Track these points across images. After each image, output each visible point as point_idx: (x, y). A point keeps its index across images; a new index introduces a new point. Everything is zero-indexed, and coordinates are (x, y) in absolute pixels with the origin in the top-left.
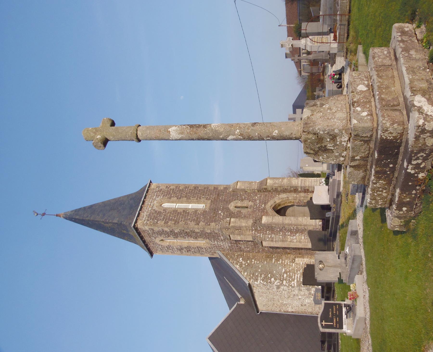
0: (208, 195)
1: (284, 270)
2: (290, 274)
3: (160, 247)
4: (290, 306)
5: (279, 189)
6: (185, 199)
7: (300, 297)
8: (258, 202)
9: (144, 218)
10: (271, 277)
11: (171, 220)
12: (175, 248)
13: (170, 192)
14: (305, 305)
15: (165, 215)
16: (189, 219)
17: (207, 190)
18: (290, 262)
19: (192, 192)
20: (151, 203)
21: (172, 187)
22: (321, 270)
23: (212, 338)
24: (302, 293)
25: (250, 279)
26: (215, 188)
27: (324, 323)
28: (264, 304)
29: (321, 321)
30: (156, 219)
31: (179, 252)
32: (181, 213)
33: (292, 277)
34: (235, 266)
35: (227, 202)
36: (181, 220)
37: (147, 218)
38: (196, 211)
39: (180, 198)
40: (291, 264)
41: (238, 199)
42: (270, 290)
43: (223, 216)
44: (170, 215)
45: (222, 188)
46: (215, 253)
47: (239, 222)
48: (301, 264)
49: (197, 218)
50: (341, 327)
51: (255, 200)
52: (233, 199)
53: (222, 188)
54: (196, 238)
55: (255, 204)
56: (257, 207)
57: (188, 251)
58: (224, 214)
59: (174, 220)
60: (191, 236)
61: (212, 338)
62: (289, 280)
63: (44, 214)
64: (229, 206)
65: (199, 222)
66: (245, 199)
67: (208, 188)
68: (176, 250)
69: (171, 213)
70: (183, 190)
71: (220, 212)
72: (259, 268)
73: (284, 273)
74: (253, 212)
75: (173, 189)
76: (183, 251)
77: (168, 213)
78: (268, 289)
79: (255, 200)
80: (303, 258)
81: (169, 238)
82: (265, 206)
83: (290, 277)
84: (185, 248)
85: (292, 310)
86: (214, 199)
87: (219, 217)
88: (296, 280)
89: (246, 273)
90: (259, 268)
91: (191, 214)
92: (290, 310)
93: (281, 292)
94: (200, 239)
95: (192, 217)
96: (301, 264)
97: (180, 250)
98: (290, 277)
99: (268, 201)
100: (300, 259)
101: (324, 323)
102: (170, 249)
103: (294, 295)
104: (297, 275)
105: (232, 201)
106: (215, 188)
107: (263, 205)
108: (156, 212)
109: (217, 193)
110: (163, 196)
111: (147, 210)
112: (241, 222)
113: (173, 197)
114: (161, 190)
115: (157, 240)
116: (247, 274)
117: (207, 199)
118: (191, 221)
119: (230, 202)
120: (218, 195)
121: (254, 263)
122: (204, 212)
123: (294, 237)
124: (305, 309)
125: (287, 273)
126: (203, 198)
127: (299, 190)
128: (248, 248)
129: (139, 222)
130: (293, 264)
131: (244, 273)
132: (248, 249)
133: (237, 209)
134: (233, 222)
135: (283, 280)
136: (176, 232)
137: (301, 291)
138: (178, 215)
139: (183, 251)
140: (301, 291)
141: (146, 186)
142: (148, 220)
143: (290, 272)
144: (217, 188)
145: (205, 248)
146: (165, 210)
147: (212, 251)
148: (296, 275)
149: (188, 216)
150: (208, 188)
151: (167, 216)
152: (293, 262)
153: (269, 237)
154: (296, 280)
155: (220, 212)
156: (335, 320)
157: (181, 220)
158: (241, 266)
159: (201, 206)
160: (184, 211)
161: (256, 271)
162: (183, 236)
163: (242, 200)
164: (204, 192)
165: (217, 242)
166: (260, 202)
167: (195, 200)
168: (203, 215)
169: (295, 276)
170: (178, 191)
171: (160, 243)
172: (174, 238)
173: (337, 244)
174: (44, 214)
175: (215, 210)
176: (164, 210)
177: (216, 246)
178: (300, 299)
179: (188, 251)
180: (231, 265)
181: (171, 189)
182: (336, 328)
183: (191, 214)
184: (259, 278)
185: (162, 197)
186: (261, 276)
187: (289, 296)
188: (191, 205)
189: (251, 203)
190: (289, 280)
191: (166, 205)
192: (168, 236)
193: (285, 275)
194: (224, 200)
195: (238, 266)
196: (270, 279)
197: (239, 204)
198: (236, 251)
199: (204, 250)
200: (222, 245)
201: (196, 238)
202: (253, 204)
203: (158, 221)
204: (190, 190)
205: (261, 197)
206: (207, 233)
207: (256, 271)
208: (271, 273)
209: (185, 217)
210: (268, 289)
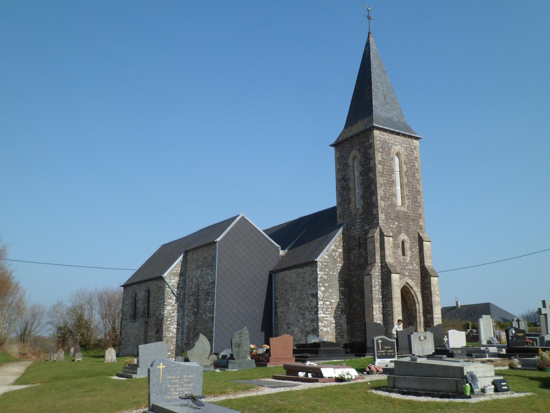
0: (412, 208)
1: (333, 301)
2: (330, 308)
3: (346, 155)
4: (285, 310)
5: (427, 292)
7: (301, 321)
8: (411, 267)
9: (382, 136)
10: (325, 287)
11: (383, 168)
12: (346, 172)
13: (411, 162)
14: (289, 328)
15: (387, 160)
16: (386, 189)
17: (417, 206)
18: (342, 308)
19: (414, 188)
20: (399, 142)
22: (420, 337)
24: (308, 324)
25: (322, 262)
26: (421, 215)
27: (380, 341)
28: (286, 279)
29: (381, 339)
30: (382, 150)
31: (341, 177)
32: (391, 178)
33: (327, 311)
34: (333, 244)
36: (384, 180)
37: (382, 139)
38: (395, 195)
40: (340, 310)
41: (411, 243)
42: (308, 286)
43: (392, 228)
44: (387, 166)
45: (421, 223)
46: (344, 219)
47: (389, 247)
48: (341, 321)
49: (388, 198)
50: (379, 357)
51: (412, 264)
52: (411, 237)
53: (421, 223)
54: (363, 197)
55: (407, 264)
56: (405, 266)
57: (343, 187)
58: (395, 228)
59: (383, 171)
60: (364, 192)
62: (324, 308)
63: (369, 18)
64: (403, 234)
65: (384, 201)
66: (412, 252)
67: (420, 206)
68: (344, 174)
69: (390, 166)
70: (415, 177)
71: (396, 223)
72: (333, 272)
73: (331, 302)
74: (400, 263)
75: (414, 166)
76: (342, 182)
77: (390, 163)
78: (310, 284)
79: (412, 264)
80: (347, 324)
81: (360, 166)
82: (408, 276)
84: (348, 185)
85: (279, 313)
86: (409, 216)
87: (390, 222)
88: (324, 315)
89: (326, 257)
90: (333, 272)
91: (391, 190)
92: (279, 310)
93: (306, 298)
94: (361, 202)
95: (388, 192)
96: (341, 321)
97: (343, 178)
98: (327, 309)
99: (412, 279)
100: (345, 320)
101: (380, 341)
102: (343, 167)
103: (304, 315)
104: (330, 317)
105: (409, 237)
106: (421, 215)
107: (407, 274)
108: (390, 149)
109: (416, 218)
110: (406, 155)
111: (390, 138)
112: (389, 249)
113: (407, 167)
114: (413, 152)
115: (354, 152)
116: (326, 259)
117: (408, 207)
118: (384, 191)
119: (408, 234)
120: (414, 220)
121: (338, 266)
123: (378, 312)
124: (282, 328)
125: (330, 305)
126: (409, 202)
127: (429, 316)
128: (355, 258)
130: (339, 312)
131: (327, 255)
132: (352, 258)
133: (400, 243)
134: (388, 240)
135: (324, 301)
136: (370, 174)
137: (312, 323)
138: (389, 175)
139: (342, 182)
140: (312, 323)
141: (412, 132)
142: (380, 141)
144: (420, 218)
145: (349, 208)
146: (392, 159)
147: (345, 216)
148: (329, 316)
149: (389, 186)
151: (387, 162)
152: (342, 312)
153: (376, 283)
154: (324, 315)
155: (396, 223)
156: (383, 351)
157: (384, 180)
158: (334, 251)
161: (330, 269)
162: (364, 183)
164: (416, 203)
165: (360, 222)
166: (411, 270)
169: (328, 314)
170: (413, 171)
171: (352, 155)
172: (361, 172)
174: (369, 18)
175: (397, 217)
176: (392, 158)
177: (354, 221)
178: (298, 321)
179: (343, 187)
180: (334, 239)
181: (414, 163)
182: (378, 353)
183: (391, 190)
184: (323, 273)
185: (405, 153)
186: (325, 275)
187: (301, 309)
188: (399, 188)
189: (408, 259)
190: (324, 308)
192: (362, 166)
193: (328, 303)
194: (408, 228)
195: (333, 247)
196: (323, 286)
197: (407, 246)
198: (348, 244)
199: (346, 207)
200: (356, 228)
201: (364, 197)
202: (408, 261)
203: (381, 152)
204: (416, 186)
205: (416, 270)
206: (372, 210)
209: (388, 184)
210: (310, 284)
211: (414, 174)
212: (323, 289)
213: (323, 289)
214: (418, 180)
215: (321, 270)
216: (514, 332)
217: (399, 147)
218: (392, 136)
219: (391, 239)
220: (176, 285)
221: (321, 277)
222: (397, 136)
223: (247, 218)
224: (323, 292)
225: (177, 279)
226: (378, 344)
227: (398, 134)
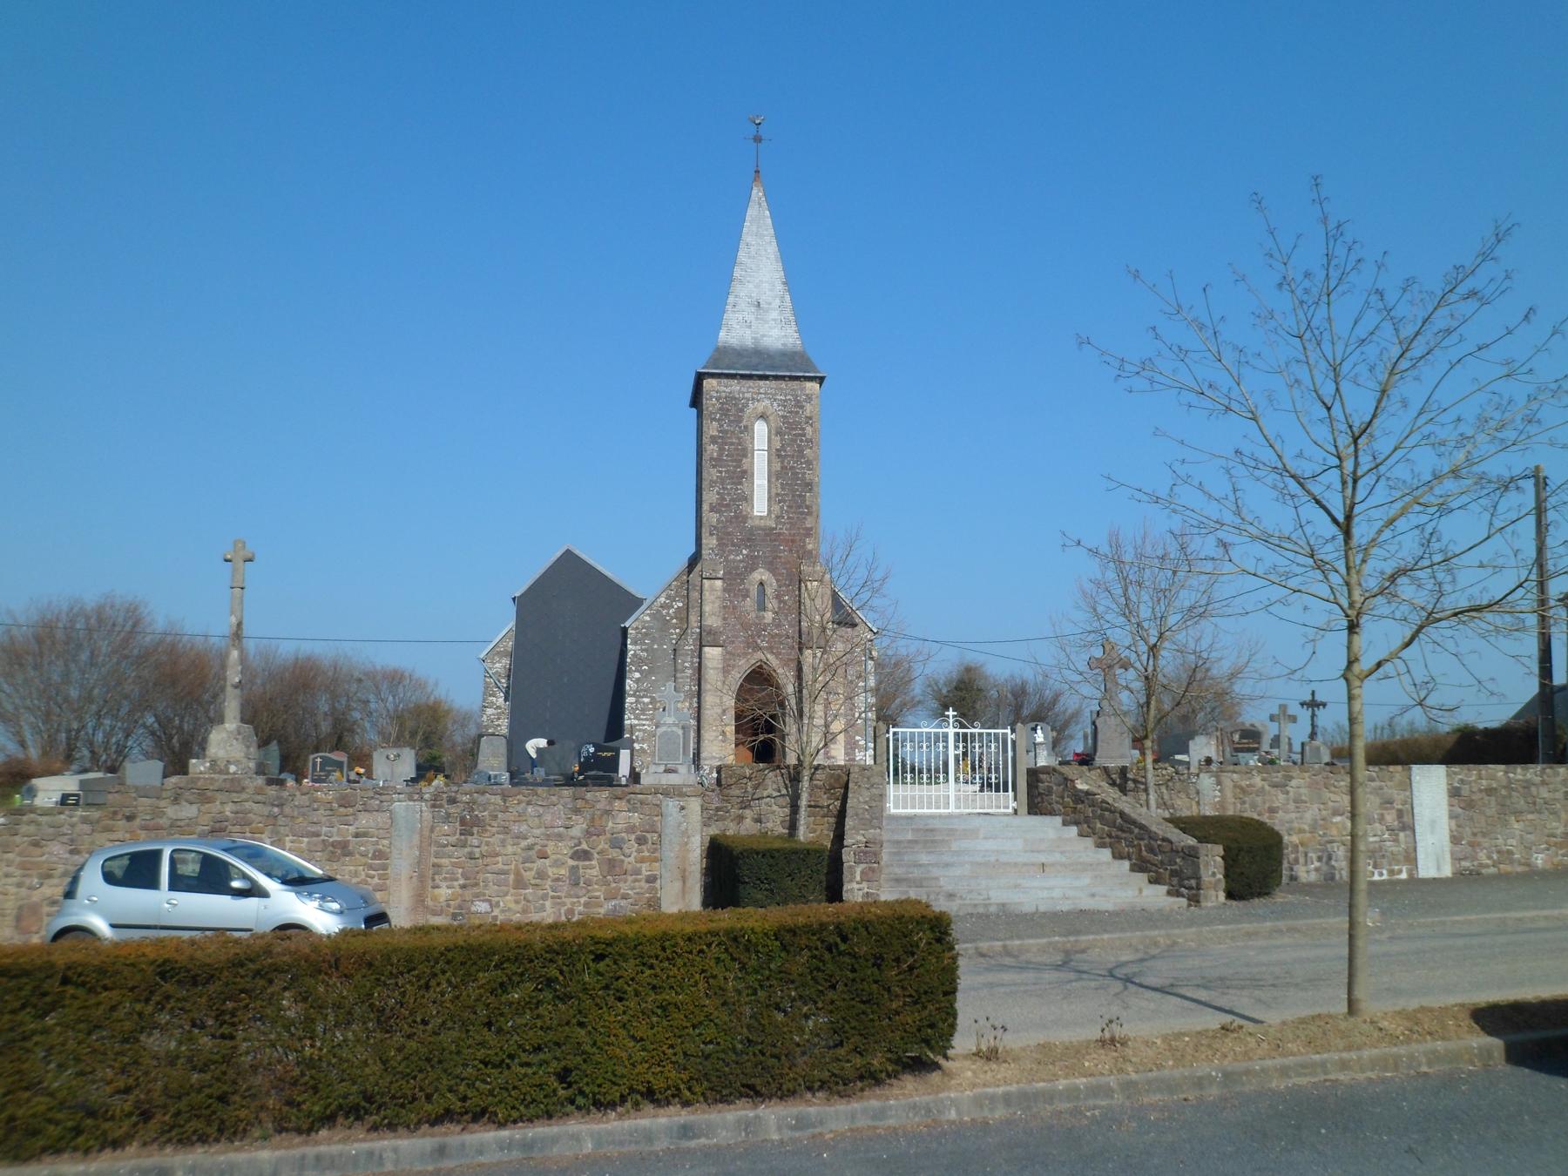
6: (777, 466)
11: (721, 449)
21: (809, 430)
23: (568, 552)
35: (771, 563)
38: (747, 499)
39: (779, 456)
49: (728, 505)
59: (720, 455)
61: (568, 552)
63: (758, 139)
70: (803, 456)
72: (661, 645)
73: (653, 698)
83: (643, 711)
90: (661, 645)
99: (777, 655)
108: (742, 410)
114: (802, 407)
122: (741, 518)
129: (714, 382)
143: (655, 709)
146: (748, 429)
150: (809, 513)
159: (760, 506)
160: (745, 472)
161: (654, 641)
163: (778, 597)
167: (774, 491)
168: (736, 517)
173: (366, 749)
174: (758, 139)
189: (769, 616)
191: (761, 430)
193: (646, 700)
197: (769, 591)
207: (654, 641)
208: (651, 672)
211: (801, 451)
212: (637, 675)
213: (637, 675)
214: (809, 463)
215: (635, 643)
216: (592, 750)
217: (767, 402)
218: (751, 383)
219: (719, 583)
220: (502, 671)
221: (635, 655)
222: (761, 383)
223: (577, 552)
224: (637, 681)
225: (506, 661)
226: (315, 764)
227: (765, 378)
